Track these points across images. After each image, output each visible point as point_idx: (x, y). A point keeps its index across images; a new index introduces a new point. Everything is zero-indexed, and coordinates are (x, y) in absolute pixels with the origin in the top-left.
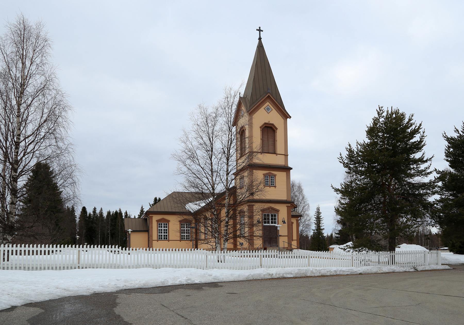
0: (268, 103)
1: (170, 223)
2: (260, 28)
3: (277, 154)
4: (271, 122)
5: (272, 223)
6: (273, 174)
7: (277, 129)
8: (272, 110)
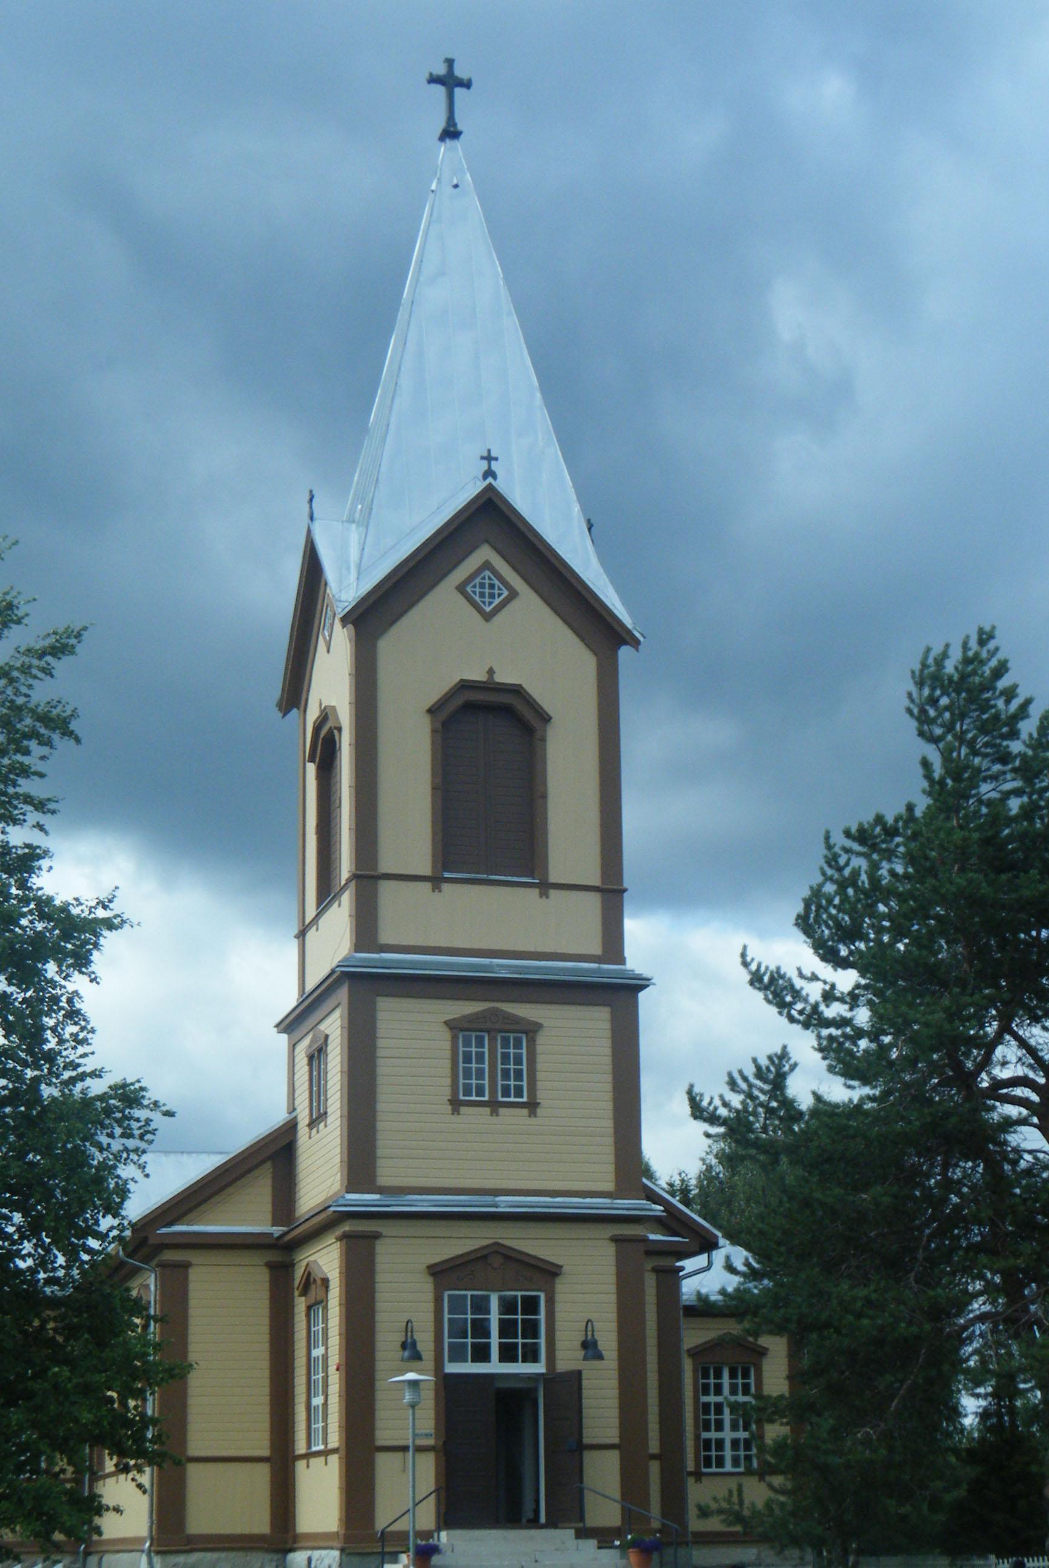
0: (485, 553)
1: (562, 1287)
2: (450, 62)
3: (545, 887)
4: (505, 677)
5: (508, 1354)
6: (516, 1020)
7: (546, 719)
8: (513, 594)
